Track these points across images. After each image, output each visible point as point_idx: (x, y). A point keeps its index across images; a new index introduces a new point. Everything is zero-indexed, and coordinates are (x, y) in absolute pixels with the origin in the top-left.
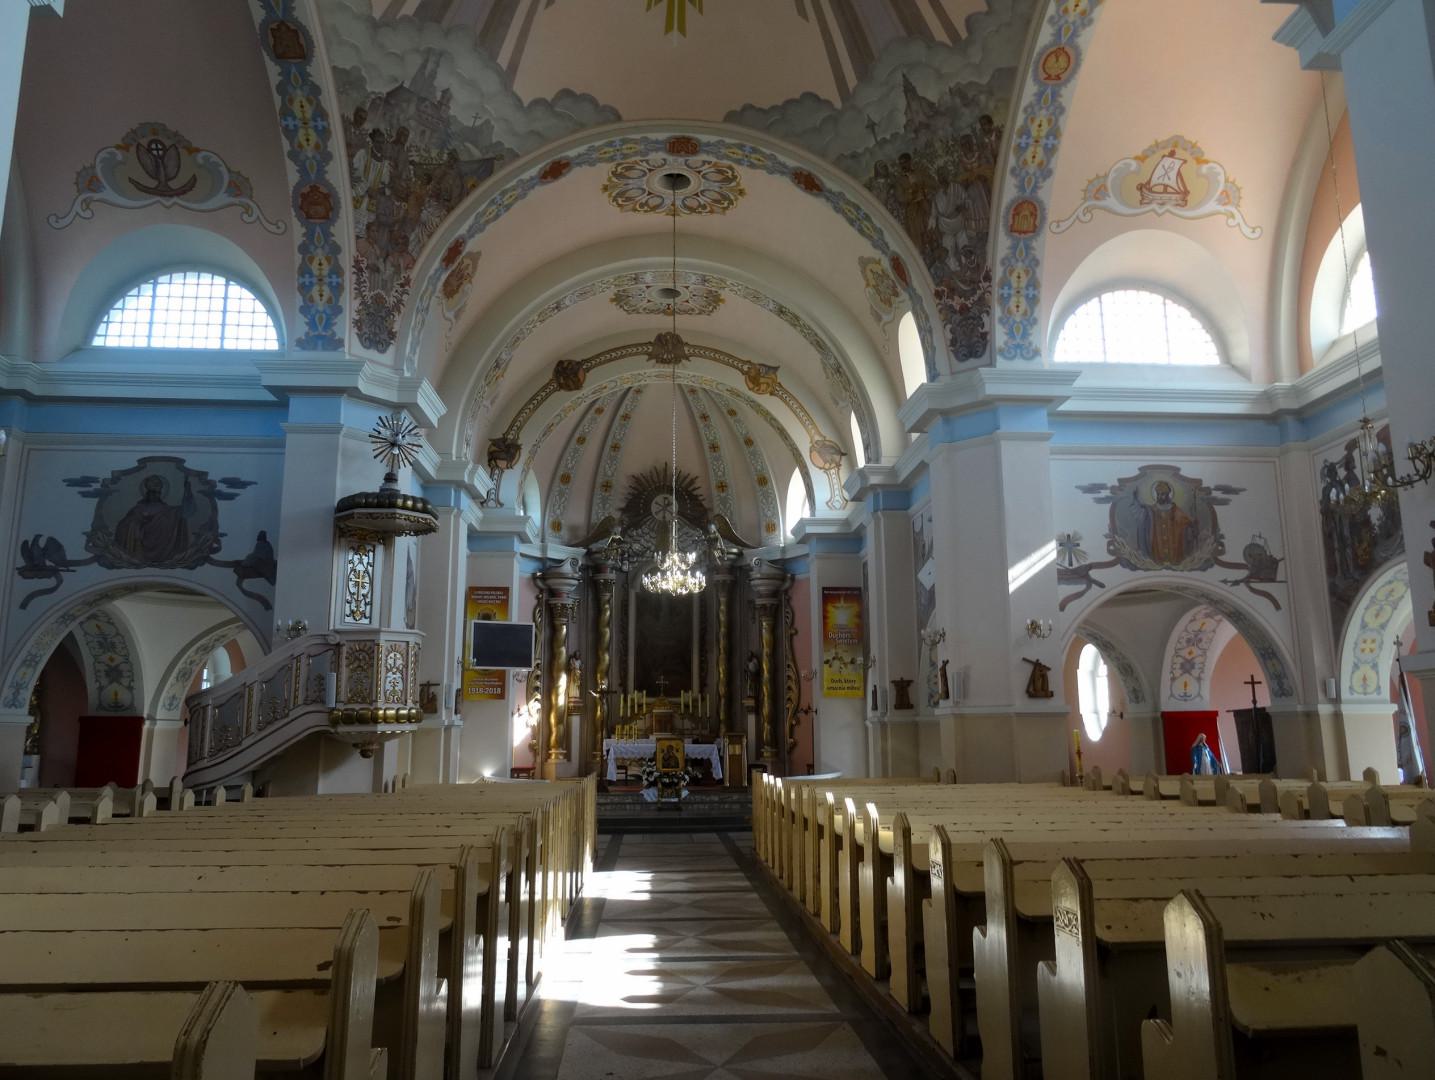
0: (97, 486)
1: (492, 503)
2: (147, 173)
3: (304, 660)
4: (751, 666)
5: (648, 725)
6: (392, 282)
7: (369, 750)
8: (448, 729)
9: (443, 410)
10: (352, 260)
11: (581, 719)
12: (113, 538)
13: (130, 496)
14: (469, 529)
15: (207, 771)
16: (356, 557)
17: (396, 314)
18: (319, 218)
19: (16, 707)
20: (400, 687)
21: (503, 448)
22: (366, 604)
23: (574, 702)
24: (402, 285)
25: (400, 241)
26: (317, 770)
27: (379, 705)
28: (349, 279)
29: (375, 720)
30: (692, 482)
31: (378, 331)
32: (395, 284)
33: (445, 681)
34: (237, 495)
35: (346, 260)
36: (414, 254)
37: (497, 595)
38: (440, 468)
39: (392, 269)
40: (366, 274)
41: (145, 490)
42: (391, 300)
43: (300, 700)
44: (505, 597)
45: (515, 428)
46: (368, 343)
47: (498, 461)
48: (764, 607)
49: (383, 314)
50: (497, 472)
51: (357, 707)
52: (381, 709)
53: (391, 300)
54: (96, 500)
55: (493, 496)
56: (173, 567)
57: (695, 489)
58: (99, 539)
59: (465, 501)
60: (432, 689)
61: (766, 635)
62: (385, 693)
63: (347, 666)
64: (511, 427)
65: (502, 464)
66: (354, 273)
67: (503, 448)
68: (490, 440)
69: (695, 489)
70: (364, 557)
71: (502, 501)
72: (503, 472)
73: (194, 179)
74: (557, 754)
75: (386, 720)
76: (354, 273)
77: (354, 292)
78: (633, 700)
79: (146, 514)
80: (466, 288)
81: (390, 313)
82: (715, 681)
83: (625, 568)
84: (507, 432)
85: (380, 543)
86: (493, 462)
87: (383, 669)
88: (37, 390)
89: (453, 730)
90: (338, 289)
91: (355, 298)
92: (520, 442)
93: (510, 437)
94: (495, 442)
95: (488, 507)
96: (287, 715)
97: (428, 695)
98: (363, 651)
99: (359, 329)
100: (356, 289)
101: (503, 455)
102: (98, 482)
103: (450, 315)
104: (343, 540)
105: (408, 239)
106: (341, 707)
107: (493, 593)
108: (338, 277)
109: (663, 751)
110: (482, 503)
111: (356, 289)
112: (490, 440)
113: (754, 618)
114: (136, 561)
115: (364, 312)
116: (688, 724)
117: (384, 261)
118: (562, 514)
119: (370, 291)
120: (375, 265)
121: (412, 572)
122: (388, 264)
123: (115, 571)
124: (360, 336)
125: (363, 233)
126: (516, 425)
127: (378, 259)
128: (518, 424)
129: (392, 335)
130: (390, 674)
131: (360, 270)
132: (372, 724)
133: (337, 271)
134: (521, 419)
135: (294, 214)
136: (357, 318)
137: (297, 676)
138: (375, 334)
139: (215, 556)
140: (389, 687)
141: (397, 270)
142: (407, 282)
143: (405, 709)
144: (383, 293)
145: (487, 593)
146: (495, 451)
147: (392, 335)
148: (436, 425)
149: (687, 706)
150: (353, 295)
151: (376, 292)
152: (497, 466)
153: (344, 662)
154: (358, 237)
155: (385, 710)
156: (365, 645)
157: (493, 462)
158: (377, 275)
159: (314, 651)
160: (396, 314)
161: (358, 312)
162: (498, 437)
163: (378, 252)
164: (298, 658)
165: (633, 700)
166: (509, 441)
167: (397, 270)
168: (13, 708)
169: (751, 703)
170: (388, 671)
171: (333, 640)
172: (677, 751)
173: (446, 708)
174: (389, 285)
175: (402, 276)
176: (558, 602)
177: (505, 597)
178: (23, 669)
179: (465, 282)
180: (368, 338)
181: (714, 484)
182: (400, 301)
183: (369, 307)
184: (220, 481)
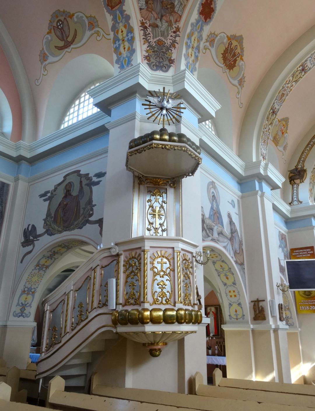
0: (49, 195)
1: (295, 203)
2: (60, 39)
3: (98, 270)
6: (168, 30)
7: (155, 350)
8: (276, 331)
9: (218, 107)
10: (139, 22)
11: (295, 169)
12: (53, 219)
13: (61, 194)
14: (272, 204)
15: (44, 362)
16: (153, 198)
17: (173, 49)
18: (117, 5)
19: (23, 316)
20: (168, 288)
21: (296, 173)
22: (163, 231)
24: (174, 32)
25: (169, 6)
26: (124, 365)
27: (147, 306)
28: (138, 33)
29: (142, 321)
31: (161, 60)
32: (170, 32)
33: (269, 298)
34: (100, 181)
35: (135, 22)
36: (180, 13)
37: (308, 251)
38: (246, 169)
39: (167, 24)
40: (150, 30)
41: (65, 191)
42: (168, 42)
43: (95, 304)
44: (312, 252)
45: (301, 162)
46: (155, 68)
47: (295, 181)
49: (164, 50)
50: (295, 186)
51: (129, 308)
52: (147, 310)
53: (168, 42)
54: (48, 201)
55: (295, 199)
56: (73, 229)
58: (48, 221)
59: (266, 188)
60: (261, 304)
62: (153, 295)
63: (124, 272)
64: (299, 161)
65: (297, 181)
66: (141, 30)
67: (296, 173)
68: (289, 171)
70: (158, 197)
71: (300, 200)
72: (298, 185)
73: (76, 31)
75: (154, 321)
76: (141, 30)
77: (143, 41)
79: (65, 203)
80: (240, 64)
81: (168, 49)
84: (298, 165)
85: (171, 187)
86: (292, 182)
87: (149, 274)
88: (28, 155)
89: (280, 332)
90: (132, 40)
91: (144, 44)
92: (305, 168)
93: (300, 167)
94: (291, 172)
95: (293, 205)
96: (87, 318)
97: (259, 308)
98: (135, 258)
99: (149, 60)
100: (143, 39)
101: (298, 177)
102: (49, 193)
103: (236, 82)
104: (142, 187)
105: (174, 4)
106: (120, 308)
107: (305, 250)
108: (131, 34)
110: (290, 204)
111: (143, 39)
112: (289, 171)
114: (60, 229)
115: (151, 51)
117: (161, 20)
119: (153, 39)
120: (154, 24)
121: (236, 231)
122: (164, 21)
123: (53, 236)
124: (149, 65)
125: (144, 6)
126: (302, 159)
127: (156, 19)
128: (302, 159)
129: (171, 61)
130: (158, 277)
131: (146, 28)
132: (140, 324)
133: (131, 30)
134: (304, 156)
135: (105, 11)
136: (147, 54)
137: (94, 284)
138: (160, 62)
139: (91, 219)
140: (157, 289)
141: (170, 24)
142: (178, 29)
143: (172, 310)
144: (163, 39)
145: (301, 251)
146: (292, 176)
147: (171, 61)
148: (214, 116)
150: (142, 43)
151: (158, 38)
152: (295, 183)
153: (122, 269)
154: (141, 9)
155: (151, 311)
156: (136, 253)
157: (292, 182)
158: (156, 28)
159: (105, 262)
160: (173, 49)
161: (147, 51)
162: (293, 169)
163: (156, 16)
164: (94, 269)
166: (299, 169)
167: (170, 24)
168: (21, 317)
170: (155, 274)
171: (114, 252)
173: (272, 316)
174: (166, 34)
175: (173, 26)
177: (312, 252)
178: (24, 296)
179: (238, 59)
180: (156, 66)
182: (174, 41)
183: (154, 48)
184: (94, 176)
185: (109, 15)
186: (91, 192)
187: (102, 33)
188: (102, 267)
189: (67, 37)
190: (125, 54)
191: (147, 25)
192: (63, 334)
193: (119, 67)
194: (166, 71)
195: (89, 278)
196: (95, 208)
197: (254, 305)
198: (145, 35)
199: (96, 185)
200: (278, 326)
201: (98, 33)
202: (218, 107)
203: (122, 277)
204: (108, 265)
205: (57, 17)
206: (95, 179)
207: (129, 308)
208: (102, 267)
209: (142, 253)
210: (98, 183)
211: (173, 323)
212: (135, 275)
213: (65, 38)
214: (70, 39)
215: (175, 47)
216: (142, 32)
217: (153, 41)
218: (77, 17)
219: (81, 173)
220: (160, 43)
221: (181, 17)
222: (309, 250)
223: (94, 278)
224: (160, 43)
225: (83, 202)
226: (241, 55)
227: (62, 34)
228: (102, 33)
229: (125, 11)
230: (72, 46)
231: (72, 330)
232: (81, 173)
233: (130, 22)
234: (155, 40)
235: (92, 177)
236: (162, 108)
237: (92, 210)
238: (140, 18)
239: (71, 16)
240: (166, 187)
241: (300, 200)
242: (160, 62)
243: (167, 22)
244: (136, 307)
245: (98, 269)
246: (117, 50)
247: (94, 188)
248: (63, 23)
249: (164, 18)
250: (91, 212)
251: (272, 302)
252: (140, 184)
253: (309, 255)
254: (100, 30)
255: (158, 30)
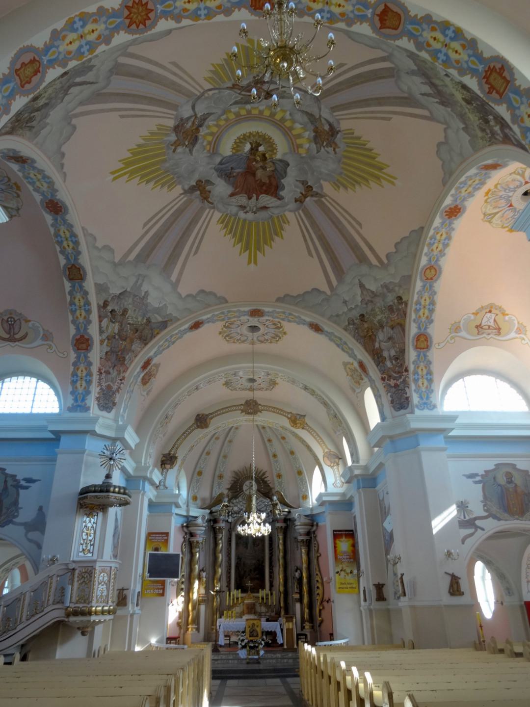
1: (162, 487)
4: (297, 574)
5: (242, 610)
8: (132, 615)
22: (91, 545)
23: (202, 597)
24: (121, 380)
25: (121, 359)
28: (95, 378)
29: (90, 613)
30: (264, 474)
31: (107, 402)
35: (95, 369)
40: (104, 375)
43: (51, 602)
44: (166, 538)
46: (102, 408)
48: (302, 541)
51: (81, 605)
53: (115, 387)
57: (265, 478)
61: (304, 557)
64: (173, 447)
65: (168, 466)
69: (265, 478)
73: (27, 334)
74: (192, 628)
75: (96, 613)
77: (97, 384)
78: (233, 595)
81: (114, 393)
82: (278, 583)
83: (230, 520)
84: (171, 451)
87: (96, 583)
90: (89, 383)
92: (177, 455)
93: (172, 452)
94: (164, 456)
99: (99, 401)
101: (168, 462)
104: (81, 510)
106: (73, 605)
109: (249, 627)
113: (298, 547)
116: (263, 609)
118: (197, 492)
120: (108, 371)
122: (115, 370)
124: (98, 405)
125: (104, 356)
126: (175, 446)
128: (176, 446)
129: (114, 404)
131: (101, 373)
132: (88, 616)
133: (90, 374)
136: (98, 396)
138: (106, 404)
141: (119, 373)
142: (124, 378)
143: (107, 606)
147: (114, 404)
149: (263, 599)
152: (165, 468)
153: (76, 579)
154: (101, 358)
159: (61, 573)
160: (117, 394)
161: (99, 393)
164: (51, 577)
165: (233, 595)
166: (171, 455)
167: (119, 373)
169: (297, 596)
171: (71, 566)
172: (257, 626)
173: (132, 603)
176: (194, 539)
177: (166, 538)
181: (275, 474)
182: (119, 388)
183: (104, 391)
184: (23, 480)
185: (73, 352)
186: (18, 494)
187: (54, 348)
188: (58, 576)
189: (15, 334)
190: (80, 390)
191: (103, 371)
192: (18, 623)
193: (73, 399)
194: (109, 412)
195: (45, 583)
196: (20, 511)
197: (119, 593)
198: (100, 379)
199: (24, 489)
200: (135, 611)
201: (50, 347)
202: (137, 440)
203: (76, 584)
204: (64, 575)
205: (11, 314)
206: (23, 483)
207: (81, 605)
208: (58, 576)
209: (94, 571)
210: (27, 488)
211: (86, 615)
212: (86, 584)
213: (12, 334)
214: (17, 336)
215: (118, 392)
216: (98, 376)
217: (104, 385)
218: (33, 325)
219: (6, 472)
220: (109, 387)
221: (128, 368)
222: (164, 535)
223: (51, 583)
224: (109, 387)
225: (6, 502)
226: (155, 376)
227: (10, 329)
228: (54, 348)
229: (89, 357)
230: (17, 343)
231: (27, 620)
232: (6, 472)
233: (91, 367)
234: (106, 384)
235: (19, 480)
236: (111, 459)
237: (18, 512)
238: (99, 365)
239: (27, 321)
240: (98, 511)
241: (167, 485)
242: (106, 404)
243: (117, 371)
244: (85, 605)
245: (54, 577)
246: (74, 383)
247: (22, 492)
248: (15, 321)
249: (116, 367)
250: (16, 514)
251: (134, 590)
252: (81, 508)
253: (163, 540)
254: (53, 344)
255: (110, 376)
